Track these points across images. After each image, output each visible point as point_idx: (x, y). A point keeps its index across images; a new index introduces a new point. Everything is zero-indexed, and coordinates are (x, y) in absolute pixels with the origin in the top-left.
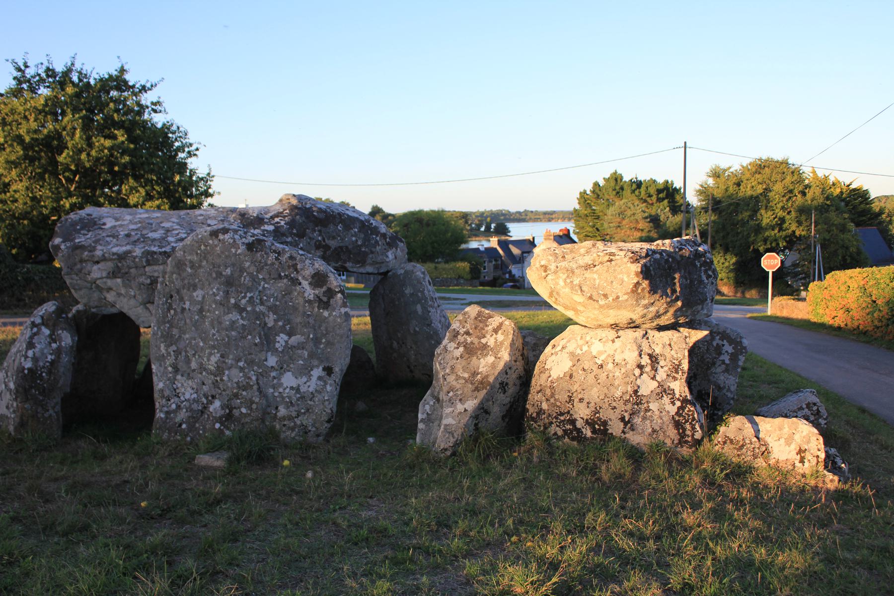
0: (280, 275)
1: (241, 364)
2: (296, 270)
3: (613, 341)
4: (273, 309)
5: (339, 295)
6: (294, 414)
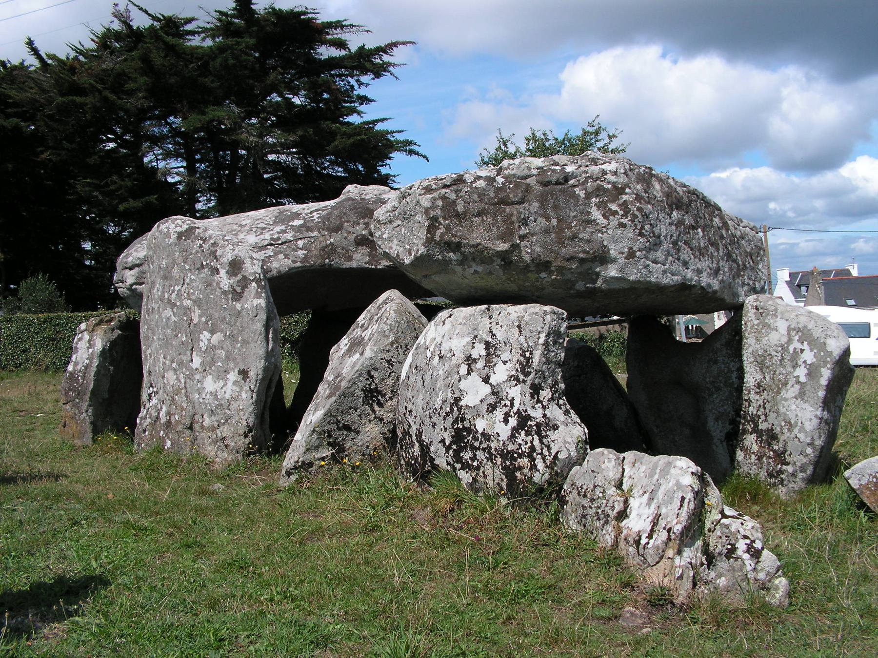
1: (174, 365)
2: (216, 257)
4: (197, 302)
5: (254, 284)
6: (216, 424)
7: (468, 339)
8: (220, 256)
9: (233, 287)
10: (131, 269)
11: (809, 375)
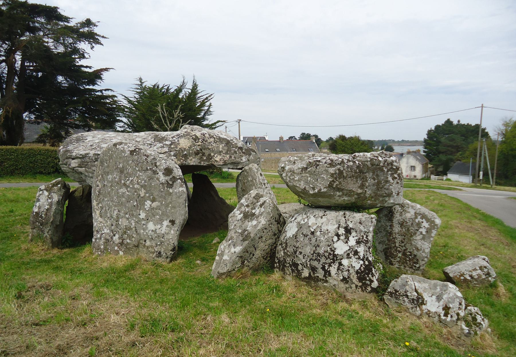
0: (147, 168)
1: (127, 216)
2: (156, 166)
3: (322, 218)
7: (337, 226)
8: (159, 166)
9: (167, 181)
10: (73, 159)
11: (427, 232)
